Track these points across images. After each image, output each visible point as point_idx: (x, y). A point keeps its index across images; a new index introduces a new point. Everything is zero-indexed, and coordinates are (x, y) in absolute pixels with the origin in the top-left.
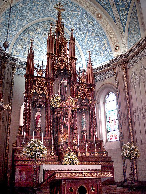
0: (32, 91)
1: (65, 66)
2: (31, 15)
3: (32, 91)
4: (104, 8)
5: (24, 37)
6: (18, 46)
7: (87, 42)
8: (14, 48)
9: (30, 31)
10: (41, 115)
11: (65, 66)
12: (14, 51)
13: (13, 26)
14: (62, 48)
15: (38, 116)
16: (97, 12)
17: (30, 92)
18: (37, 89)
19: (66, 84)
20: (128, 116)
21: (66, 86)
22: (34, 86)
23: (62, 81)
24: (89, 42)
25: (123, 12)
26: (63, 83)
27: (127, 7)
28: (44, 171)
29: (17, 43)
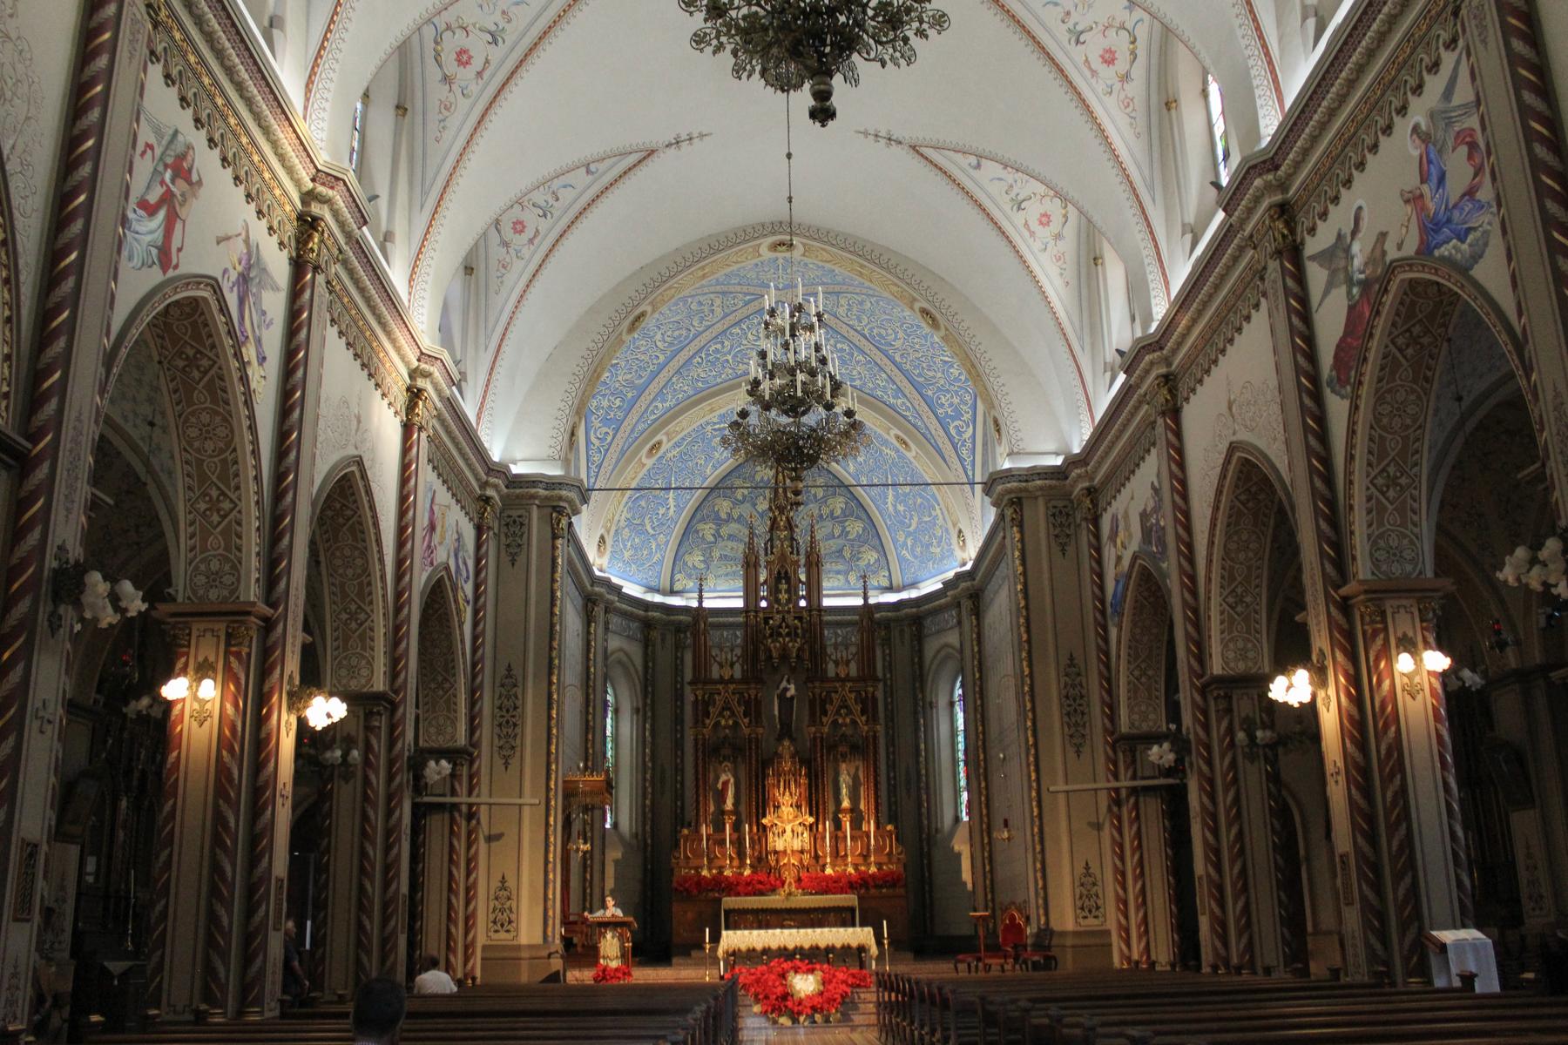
0: (707, 721)
1: (784, 648)
2: (709, 458)
3: (707, 721)
4: (909, 421)
5: (701, 526)
6: (687, 557)
7: (895, 506)
8: (677, 568)
9: (717, 501)
10: (732, 780)
11: (784, 648)
12: (678, 576)
13: (662, 511)
14: (784, 587)
15: (726, 784)
16: (917, 306)
17: (704, 724)
18: (721, 714)
19: (792, 691)
20: (918, 772)
21: (792, 698)
22: (711, 710)
23: (784, 684)
24: (901, 508)
25: (960, 433)
26: (786, 690)
27: (967, 417)
28: (1436, 575)
29: (682, 550)
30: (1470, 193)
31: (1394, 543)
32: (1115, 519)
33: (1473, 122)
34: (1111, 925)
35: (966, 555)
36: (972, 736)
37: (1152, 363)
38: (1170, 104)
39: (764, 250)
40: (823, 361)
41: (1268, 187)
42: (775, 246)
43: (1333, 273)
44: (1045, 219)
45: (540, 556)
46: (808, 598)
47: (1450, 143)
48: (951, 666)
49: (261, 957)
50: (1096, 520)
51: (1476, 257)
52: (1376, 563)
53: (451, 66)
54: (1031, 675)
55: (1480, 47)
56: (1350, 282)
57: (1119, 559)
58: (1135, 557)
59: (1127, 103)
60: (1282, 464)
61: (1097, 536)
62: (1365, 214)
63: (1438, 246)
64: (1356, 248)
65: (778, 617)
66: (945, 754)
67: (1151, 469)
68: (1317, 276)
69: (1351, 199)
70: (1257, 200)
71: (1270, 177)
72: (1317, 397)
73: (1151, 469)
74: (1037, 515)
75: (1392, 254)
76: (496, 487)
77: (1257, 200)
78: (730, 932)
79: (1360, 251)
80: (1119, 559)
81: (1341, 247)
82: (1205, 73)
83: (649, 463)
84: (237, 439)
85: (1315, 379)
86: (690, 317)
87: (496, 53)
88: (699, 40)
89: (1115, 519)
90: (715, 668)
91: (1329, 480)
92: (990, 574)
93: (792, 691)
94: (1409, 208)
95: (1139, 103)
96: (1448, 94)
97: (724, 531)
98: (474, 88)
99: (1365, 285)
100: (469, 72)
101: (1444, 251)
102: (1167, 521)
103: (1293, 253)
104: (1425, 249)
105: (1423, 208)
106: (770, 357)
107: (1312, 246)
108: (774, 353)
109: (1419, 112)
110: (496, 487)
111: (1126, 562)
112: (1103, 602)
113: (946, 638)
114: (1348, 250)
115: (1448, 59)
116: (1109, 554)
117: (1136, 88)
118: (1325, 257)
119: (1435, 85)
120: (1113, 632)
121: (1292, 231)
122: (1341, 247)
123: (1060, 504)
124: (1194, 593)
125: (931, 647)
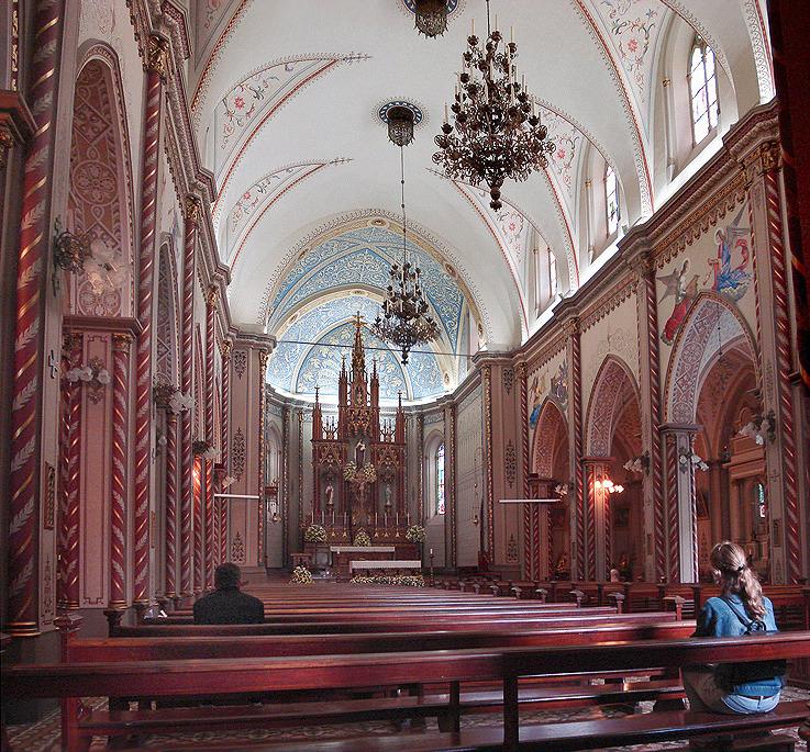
25: (451, 327)
30: (741, 268)
31: (682, 408)
32: (536, 379)
33: (748, 238)
34: (522, 563)
35: (451, 387)
36: (449, 474)
37: (569, 312)
38: (587, 183)
39: (370, 225)
40: (419, 293)
41: (643, 244)
42: (374, 222)
43: (670, 288)
44: (512, 227)
45: (254, 374)
46: (372, 401)
47: (735, 244)
48: (437, 440)
49: (30, 565)
50: (526, 379)
51: (740, 297)
52: (675, 416)
53: (232, 108)
54: (491, 449)
55: (756, 209)
56: (678, 294)
57: (537, 398)
58: (547, 399)
59: (567, 179)
60: (634, 368)
61: (526, 386)
62: (689, 265)
63: (723, 288)
64: (683, 279)
65: (357, 411)
66: (432, 483)
67: (562, 358)
68: (661, 288)
69: (683, 257)
70: (636, 248)
71: (643, 239)
72: (656, 343)
73: (562, 358)
74: (498, 374)
75: (700, 287)
76: (232, 337)
77: (636, 248)
78: (473, 565)
79: (684, 281)
80: (537, 398)
81: (675, 277)
82: (607, 165)
83: (290, 326)
84: (170, 318)
85: (656, 335)
86: (321, 252)
87: (258, 104)
88: (437, 158)
89: (536, 379)
90: (325, 434)
91: (658, 379)
92: (461, 399)
93: (363, 448)
94: (711, 268)
95: (573, 179)
96: (737, 221)
97: (325, 363)
98: (245, 121)
99: (685, 297)
100: (243, 112)
101: (726, 290)
102: (568, 384)
103: (651, 276)
104: (717, 288)
105: (718, 269)
106: (394, 290)
107: (660, 273)
108: (397, 289)
109: (721, 226)
110: (232, 337)
111: (541, 401)
112: (526, 417)
113: (436, 426)
114: (678, 279)
115: (738, 206)
116: (531, 395)
117: (572, 172)
118: (667, 280)
119: (731, 216)
120: (531, 432)
121: (651, 265)
122: (675, 277)
123: (508, 369)
124: (580, 419)
125: (428, 430)
